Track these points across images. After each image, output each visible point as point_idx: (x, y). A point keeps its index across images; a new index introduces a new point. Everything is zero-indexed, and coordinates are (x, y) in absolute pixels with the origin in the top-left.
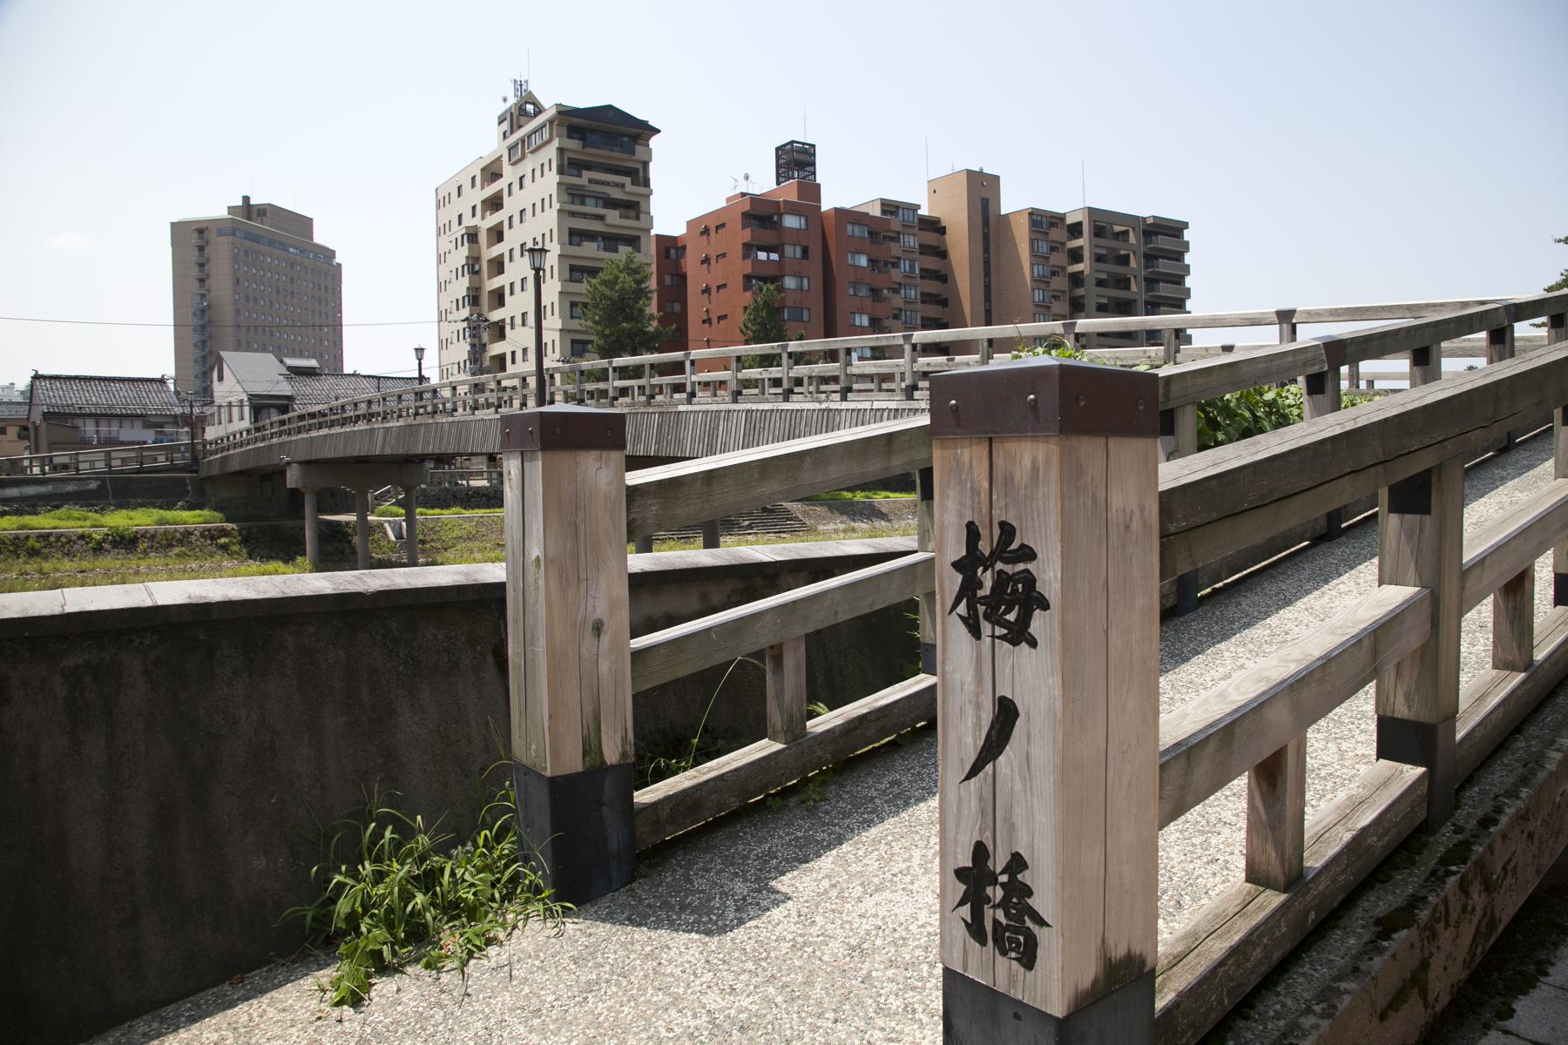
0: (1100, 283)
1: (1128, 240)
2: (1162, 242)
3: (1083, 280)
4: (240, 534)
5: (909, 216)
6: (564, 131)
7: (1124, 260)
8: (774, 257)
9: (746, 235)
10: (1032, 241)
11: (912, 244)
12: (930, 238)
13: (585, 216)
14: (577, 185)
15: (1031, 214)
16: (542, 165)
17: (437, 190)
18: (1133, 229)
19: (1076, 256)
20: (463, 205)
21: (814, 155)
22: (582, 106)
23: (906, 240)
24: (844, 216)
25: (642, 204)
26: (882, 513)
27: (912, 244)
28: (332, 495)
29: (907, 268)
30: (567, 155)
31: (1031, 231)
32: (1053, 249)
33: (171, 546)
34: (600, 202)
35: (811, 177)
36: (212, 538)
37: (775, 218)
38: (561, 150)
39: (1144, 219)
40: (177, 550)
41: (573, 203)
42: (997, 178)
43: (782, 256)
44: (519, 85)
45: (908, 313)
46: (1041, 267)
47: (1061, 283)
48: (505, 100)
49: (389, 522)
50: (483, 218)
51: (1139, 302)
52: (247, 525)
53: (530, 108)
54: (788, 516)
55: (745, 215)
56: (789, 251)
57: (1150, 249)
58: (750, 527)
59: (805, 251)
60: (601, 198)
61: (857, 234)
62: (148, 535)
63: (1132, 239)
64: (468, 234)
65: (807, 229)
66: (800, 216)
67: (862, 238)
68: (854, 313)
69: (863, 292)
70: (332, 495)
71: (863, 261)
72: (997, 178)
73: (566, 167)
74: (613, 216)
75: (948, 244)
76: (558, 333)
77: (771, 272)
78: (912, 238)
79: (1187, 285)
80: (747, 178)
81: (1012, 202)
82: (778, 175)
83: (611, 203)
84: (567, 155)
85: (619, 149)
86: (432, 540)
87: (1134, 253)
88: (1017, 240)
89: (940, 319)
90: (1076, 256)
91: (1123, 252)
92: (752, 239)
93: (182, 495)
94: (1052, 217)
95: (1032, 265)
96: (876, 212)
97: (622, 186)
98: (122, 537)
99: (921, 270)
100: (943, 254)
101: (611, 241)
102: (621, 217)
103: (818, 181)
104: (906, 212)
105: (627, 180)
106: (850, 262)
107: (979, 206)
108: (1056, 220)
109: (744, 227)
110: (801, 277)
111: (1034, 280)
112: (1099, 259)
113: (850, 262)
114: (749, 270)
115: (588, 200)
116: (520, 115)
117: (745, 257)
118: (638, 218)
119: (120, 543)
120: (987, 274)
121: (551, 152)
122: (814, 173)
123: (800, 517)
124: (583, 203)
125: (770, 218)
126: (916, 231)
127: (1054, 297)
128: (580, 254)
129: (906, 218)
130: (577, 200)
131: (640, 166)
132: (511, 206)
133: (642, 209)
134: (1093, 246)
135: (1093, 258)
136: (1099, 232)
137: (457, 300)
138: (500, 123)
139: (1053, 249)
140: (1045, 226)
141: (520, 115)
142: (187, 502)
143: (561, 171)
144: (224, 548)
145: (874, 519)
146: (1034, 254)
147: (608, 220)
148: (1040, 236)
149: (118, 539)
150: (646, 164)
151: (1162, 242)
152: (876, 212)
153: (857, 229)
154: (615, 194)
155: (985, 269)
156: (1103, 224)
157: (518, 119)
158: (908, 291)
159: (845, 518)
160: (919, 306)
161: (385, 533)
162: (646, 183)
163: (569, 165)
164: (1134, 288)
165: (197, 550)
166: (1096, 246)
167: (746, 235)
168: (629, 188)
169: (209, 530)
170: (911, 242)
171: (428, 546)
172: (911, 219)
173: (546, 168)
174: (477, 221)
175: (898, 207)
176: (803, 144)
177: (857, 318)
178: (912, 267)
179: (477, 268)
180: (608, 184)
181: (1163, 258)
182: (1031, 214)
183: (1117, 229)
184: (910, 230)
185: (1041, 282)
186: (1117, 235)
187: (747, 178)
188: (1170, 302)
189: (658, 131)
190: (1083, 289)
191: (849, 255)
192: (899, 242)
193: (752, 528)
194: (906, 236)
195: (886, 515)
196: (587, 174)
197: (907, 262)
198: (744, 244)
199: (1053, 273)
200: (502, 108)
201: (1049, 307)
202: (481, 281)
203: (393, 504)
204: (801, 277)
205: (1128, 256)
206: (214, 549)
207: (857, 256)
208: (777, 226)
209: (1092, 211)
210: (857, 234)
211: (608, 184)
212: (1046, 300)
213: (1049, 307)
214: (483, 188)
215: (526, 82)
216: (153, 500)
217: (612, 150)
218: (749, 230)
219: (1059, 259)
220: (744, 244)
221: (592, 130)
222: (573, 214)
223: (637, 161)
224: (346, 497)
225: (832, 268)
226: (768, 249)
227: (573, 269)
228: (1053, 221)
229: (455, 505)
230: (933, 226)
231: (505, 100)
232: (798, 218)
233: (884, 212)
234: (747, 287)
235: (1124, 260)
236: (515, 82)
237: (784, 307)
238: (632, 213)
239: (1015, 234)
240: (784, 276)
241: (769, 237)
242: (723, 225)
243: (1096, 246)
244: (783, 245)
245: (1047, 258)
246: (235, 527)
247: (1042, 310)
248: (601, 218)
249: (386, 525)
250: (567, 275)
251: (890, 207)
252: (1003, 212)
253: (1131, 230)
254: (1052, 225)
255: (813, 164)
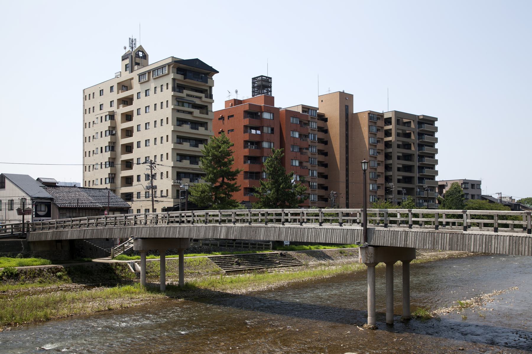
0: (399, 146)
1: (410, 126)
2: (426, 127)
3: (391, 145)
4: (66, 270)
5: (314, 113)
6: (175, 70)
7: (408, 136)
8: (259, 132)
9: (247, 121)
10: (369, 126)
11: (315, 127)
12: (321, 123)
13: (184, 112)
14: (181, 97)
15: (369, 114)
16: (162, 86)
17: (84, 90)
18: (413, 121)
19: (388, 133)
20: (106, 99)
21: (271, 82)
22: (185, 59)
23: (312, 124)
24: (289, 113)
25: (209, 107)
26: (328, 256)
27: (315, 127)
28: (90, 249)
29: (312, 138)
30: (177, 82)
31: (369, 122)
32: (378, 130)
33: (34, 277)
34: (191, 105)
35: (270, 93)
36: (53, 273)
37: (259, 114)
38: (174, 80)
39: (418, 116)
40: (38, 279)
41: (179, 105)
42: (352, 96)
43: (262, 132)
44: (132, 42)
45: (313, 159)
46: (373, 138)
47: (381, 146)
48: (125, 48)
49: (129, 263)
50: (118, 108)
51: (415, 155)
52: (68, 265)
53: (141, 54)
54: (291, 258)
55: (245, 112)
56: (265, 129)
57: (421, 130)
58: (279, 263)
59: (272, 130)
60: (191, 103)
61: (294, 122)
62: (23, 272)
63: (413, 126)
64: (110, 115)
65: (273, 119)
66: (271, 113)
67: (297, 124)
68: (293, 160)
69: (296, 150)
70: (90, 249)
71: (297, 135)
72: (352, 96)
73: (176, 88)
74: (197, 112)
75: (329, 127)
76: (171, 168)
77: (257, 139)
78: (315, 123)
79: (436, 147)
80: (237, 92)
81: (358, 108)
82: (253, 92)
83: (195, 106)
84: (177, 82)
85: (201, 80)
86: (151, 272)
87: (413, 132)
88: (362, 126)
89: (324, 162)
90: (388, 133)
91: (407, 132)
92: (250, 123)
93: (19, 250)
94: (378, 115)
95: (369, 138)
96: (300, 110)
97: (200, 98)
98: (12, 273)
99: (318, 139)
100: (326, 131)
101: (195, 124)
102: (200, 113)
103: (273, 95)
104: (312, 111)
105: (203, 95)
106: (292, 135)
107: (344, 109)
108: (380, 116)
109: (245, 117)
110: (271, 142)
111: (370, 145)
112: (398, 135)
113: (292, 135)
114: (247, 139)
115: (185, 104)
116: (136, 57)
117: (245, 132)
118: (207, 114)
119: (11, 276)
120: (347, 141)
121: (169, 79)
122: (271, 91)
123: (297, 258)
124: (183, 106)
125: (256, 114)
126: (316, 120)
127: (378, 152)
128: (182, 131)
129: (312, 114)
130: (180, 104)
131: (208, 89)
132: (136, 104)
133: (209, 109)
134: (397, 129)
135: (396, 134)
136: (398, 122)
137: (102, 148)
138: (123, 60)
139: (378, 130)
140: (375, 120)
141: (136, 57)
142: (22, 253)
143: (174, 90)
144: (60, 277)
145: (327, 259)
146: (370, 132)
147: (195, 114)
148: (372, 124)
149: (10, 274)
150: (211, 88)
151: (426, 127)
152: (300, 110)
153: (294, 119)
154: (198, 102)
155: (346, 139)
156: (400, 118)
157: (135, 59)
158: (313, 149)
159: (315, 259)
160: (317, 156)
161: (129, 268)
162: (211, 97)
163: (178, 87)
164: (413, 148)
165: (48, 279)
166: (398, 129)
167: (247, 121)
168: (204, 99)
169: (51, 269)
170: (314, 125)
171: (149, 274)
172: (315, 114)
173: (165, 87)
174: (114, 108)
175: (309, 109)
176: (266, 77)
177: (294, 162)
178: (314, 137)
179: (114, 132)
180: (193, 97)
181: (426, 134)
182: (369, 114)
183: (405, 120)
184: (313, 120)
185: (373, 145)
186: (405, 124)
187: (237, 92)
188: (428, 155)
189: (218, 72)
190: (391, 149)
191: (291, 132)
192: (309, 125)
193: (280, 264)
194: (312, 123)
195: (330, 257)
196: (186, 92)
197: (312, 135)
198: (244, 126)
199: (378, 141)
200: (123, 52)
201: (376, 157)
202: (116, 139)
203: (123, 254)
204: (271, 142)
205: (410, 133)
206: (56, 278)
207: (294, 133)
208: (260, 118)
209: (396, 112)
210: (294, 122)
211: (193, 97)
212: (375, 154)
213: (376, 157)
214: (118, 93)
215: (136, 39)
216: (7, 253)
217: (198, 81)
218: (248, 119)
219: (381, 135)
220: (244, 126)
221: (190, 71)
222: (178, 111)
223: (208, 86)
224: (97, 250)
225: (284, 138)
226: (256, 129)
227: (178, 137)
228: (378, 117)
229: (151, 254)
230: (322, 118)
231: (125, 48)
232: (269, 114)
233: (303, 111)
234: (245, 147)
235: (408, 136)
236: (130, 39)
237: (262, 157)
238: (205, 111)
239: (361, 123)
240: (263, 141)
241: (256, 123)
242: (232, 116)
243: (398, 129)
244: (263, 127)
245: (376, 134)
246: (62, 266)
247: (373, 159)
248: (191, 113)
249: (129, 264)
250: (175, 140)
251: (306, 109)
252: (354, 112)
253: (412, 121)
254: (378, 119)
255: (271, 87)
